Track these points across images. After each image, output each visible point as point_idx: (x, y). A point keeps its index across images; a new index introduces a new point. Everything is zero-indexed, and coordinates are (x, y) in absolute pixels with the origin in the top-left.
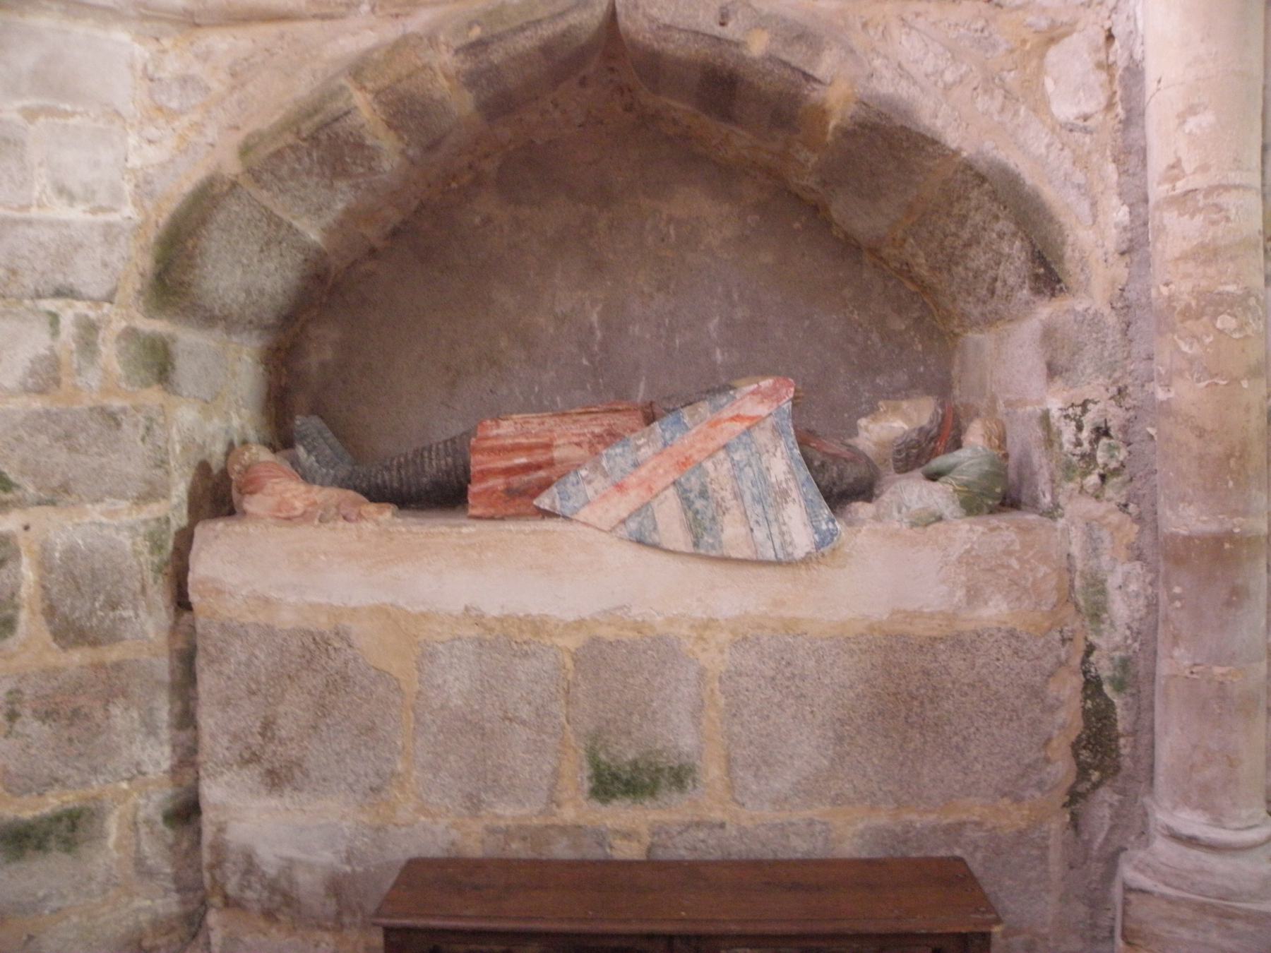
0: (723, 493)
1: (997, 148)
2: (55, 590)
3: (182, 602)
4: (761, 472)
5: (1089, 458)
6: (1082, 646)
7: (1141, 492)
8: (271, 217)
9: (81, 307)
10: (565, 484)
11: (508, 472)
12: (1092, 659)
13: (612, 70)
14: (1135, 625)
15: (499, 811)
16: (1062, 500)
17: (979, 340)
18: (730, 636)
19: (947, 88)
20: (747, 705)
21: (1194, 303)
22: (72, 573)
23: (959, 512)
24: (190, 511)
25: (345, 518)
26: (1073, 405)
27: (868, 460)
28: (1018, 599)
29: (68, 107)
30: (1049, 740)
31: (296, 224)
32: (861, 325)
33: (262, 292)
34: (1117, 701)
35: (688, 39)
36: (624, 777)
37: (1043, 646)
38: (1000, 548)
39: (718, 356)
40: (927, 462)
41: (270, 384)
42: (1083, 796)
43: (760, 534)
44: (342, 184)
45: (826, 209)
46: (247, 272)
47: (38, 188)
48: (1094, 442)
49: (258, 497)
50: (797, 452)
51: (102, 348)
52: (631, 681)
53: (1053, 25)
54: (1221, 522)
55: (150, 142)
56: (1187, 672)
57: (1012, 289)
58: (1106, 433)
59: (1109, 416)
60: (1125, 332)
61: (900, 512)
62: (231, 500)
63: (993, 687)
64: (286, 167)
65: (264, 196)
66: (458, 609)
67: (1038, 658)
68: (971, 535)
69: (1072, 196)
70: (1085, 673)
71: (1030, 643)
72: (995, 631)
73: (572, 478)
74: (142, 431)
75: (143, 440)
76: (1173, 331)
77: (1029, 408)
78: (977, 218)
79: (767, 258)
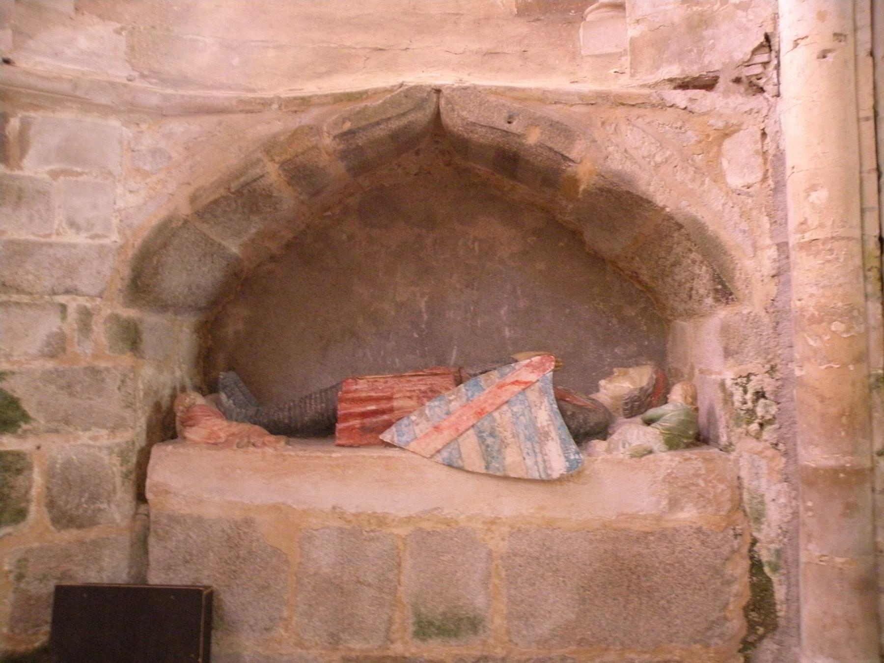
0: (506, 434)
1: (689, 206)
2: (55, 489)
3: (141, 497)
4: (530, 419)
5: (751, 412)
6: (749, 540)
7: (787, 436)
8: (208, 240)
9: (82, 301)
10: (400, 425)
11: (364, 415)
12: (755, 548)
13: (437, 142)
14: (784, 526)
15: (351, 646)
16: (734, 440)
17: (684, 325)
18: (509, 529)
19: (657, 166)
20: (520, 576)
21: (816, 313)
22: (67, 478)
23: (664, 447)
24: (148, 436)
25: (254, 445)
26: (740, 377)
27: (606, 409)
28: (704, 507)
29: (79, 170)
30: (727, 604)
31: (224, 243)
32: (604, 312)
33: (198, 287)
34: (775, 578)
35: (487, 132)
36: (437, 623)
37: (722, 540)
38: (691, 472)
39: (507, 333)
40: (646, 411)
41: (200, 346)
42: (753, 645)
43: (529, 462)
44: (255, 218)
45: (582, 234)
46: (189, 276)
47: (57, 222)
48: (755, 401)
49: (194, 429)
50: (555, 406)
51: (94, 328)
52: (442, 558)
53: (727, 126)
54: (837, 459)
55: (131, 192)
56: (817, 561)
57: (702, 297)
58: (763, 396)
59: (765, 385)
60: (775, 328)
61: (624, 447)
62: (174, 428)
63: (687, 566)
64: (220, 210)
65: (204, 227)
66: (328, 507)
67: (718, 547)
68: (671, 463)
69: (739, 238)
70: (752, 558)
71: (712, 537)
72: (688, 529)
73: (405, 421)
74: (119, 383)
75: (119, 389)
76: (804, 330)
77: (713, 377)
78: (678, 250)
79: (541, 266)
